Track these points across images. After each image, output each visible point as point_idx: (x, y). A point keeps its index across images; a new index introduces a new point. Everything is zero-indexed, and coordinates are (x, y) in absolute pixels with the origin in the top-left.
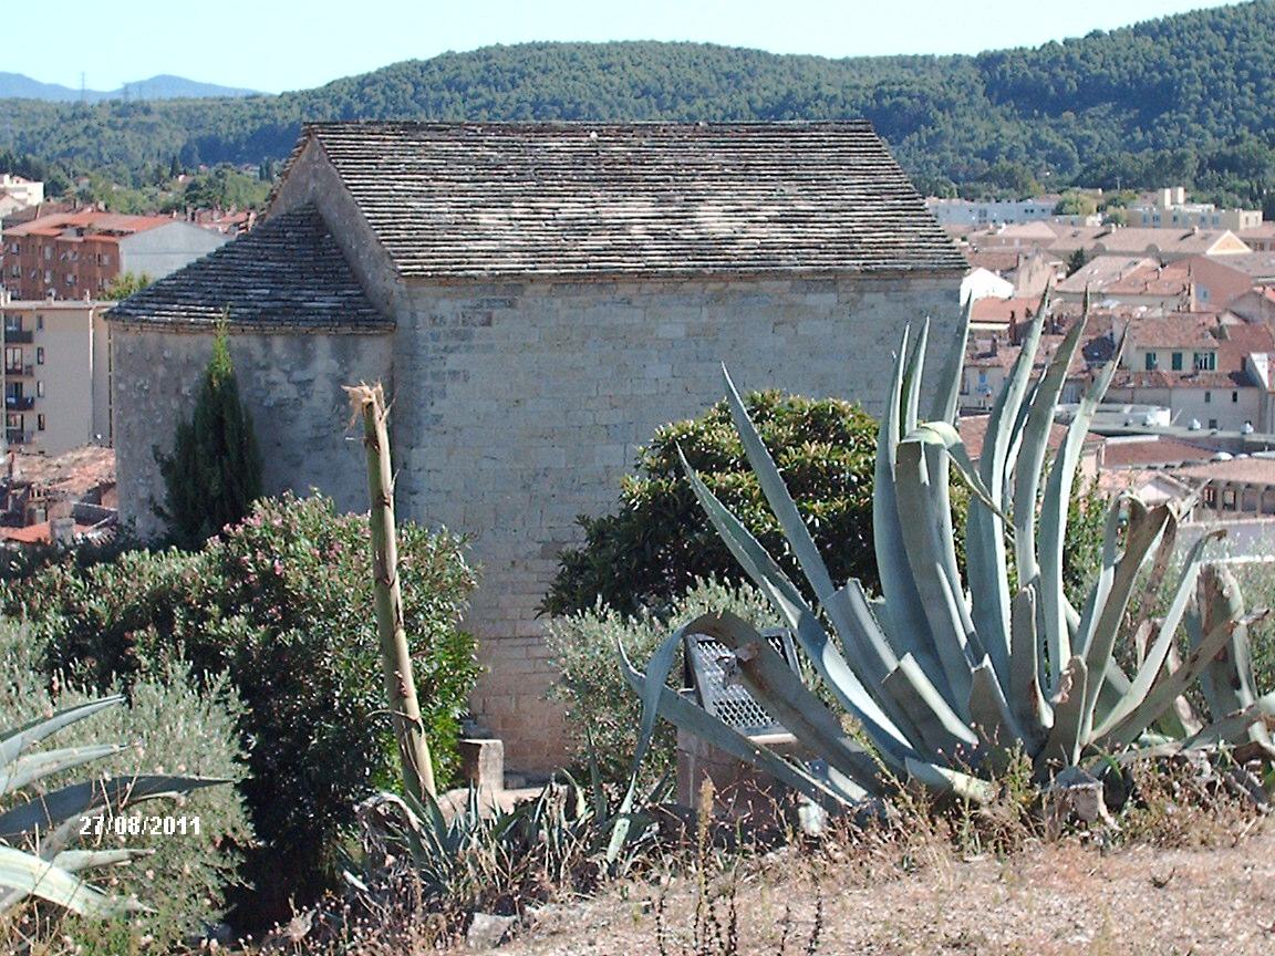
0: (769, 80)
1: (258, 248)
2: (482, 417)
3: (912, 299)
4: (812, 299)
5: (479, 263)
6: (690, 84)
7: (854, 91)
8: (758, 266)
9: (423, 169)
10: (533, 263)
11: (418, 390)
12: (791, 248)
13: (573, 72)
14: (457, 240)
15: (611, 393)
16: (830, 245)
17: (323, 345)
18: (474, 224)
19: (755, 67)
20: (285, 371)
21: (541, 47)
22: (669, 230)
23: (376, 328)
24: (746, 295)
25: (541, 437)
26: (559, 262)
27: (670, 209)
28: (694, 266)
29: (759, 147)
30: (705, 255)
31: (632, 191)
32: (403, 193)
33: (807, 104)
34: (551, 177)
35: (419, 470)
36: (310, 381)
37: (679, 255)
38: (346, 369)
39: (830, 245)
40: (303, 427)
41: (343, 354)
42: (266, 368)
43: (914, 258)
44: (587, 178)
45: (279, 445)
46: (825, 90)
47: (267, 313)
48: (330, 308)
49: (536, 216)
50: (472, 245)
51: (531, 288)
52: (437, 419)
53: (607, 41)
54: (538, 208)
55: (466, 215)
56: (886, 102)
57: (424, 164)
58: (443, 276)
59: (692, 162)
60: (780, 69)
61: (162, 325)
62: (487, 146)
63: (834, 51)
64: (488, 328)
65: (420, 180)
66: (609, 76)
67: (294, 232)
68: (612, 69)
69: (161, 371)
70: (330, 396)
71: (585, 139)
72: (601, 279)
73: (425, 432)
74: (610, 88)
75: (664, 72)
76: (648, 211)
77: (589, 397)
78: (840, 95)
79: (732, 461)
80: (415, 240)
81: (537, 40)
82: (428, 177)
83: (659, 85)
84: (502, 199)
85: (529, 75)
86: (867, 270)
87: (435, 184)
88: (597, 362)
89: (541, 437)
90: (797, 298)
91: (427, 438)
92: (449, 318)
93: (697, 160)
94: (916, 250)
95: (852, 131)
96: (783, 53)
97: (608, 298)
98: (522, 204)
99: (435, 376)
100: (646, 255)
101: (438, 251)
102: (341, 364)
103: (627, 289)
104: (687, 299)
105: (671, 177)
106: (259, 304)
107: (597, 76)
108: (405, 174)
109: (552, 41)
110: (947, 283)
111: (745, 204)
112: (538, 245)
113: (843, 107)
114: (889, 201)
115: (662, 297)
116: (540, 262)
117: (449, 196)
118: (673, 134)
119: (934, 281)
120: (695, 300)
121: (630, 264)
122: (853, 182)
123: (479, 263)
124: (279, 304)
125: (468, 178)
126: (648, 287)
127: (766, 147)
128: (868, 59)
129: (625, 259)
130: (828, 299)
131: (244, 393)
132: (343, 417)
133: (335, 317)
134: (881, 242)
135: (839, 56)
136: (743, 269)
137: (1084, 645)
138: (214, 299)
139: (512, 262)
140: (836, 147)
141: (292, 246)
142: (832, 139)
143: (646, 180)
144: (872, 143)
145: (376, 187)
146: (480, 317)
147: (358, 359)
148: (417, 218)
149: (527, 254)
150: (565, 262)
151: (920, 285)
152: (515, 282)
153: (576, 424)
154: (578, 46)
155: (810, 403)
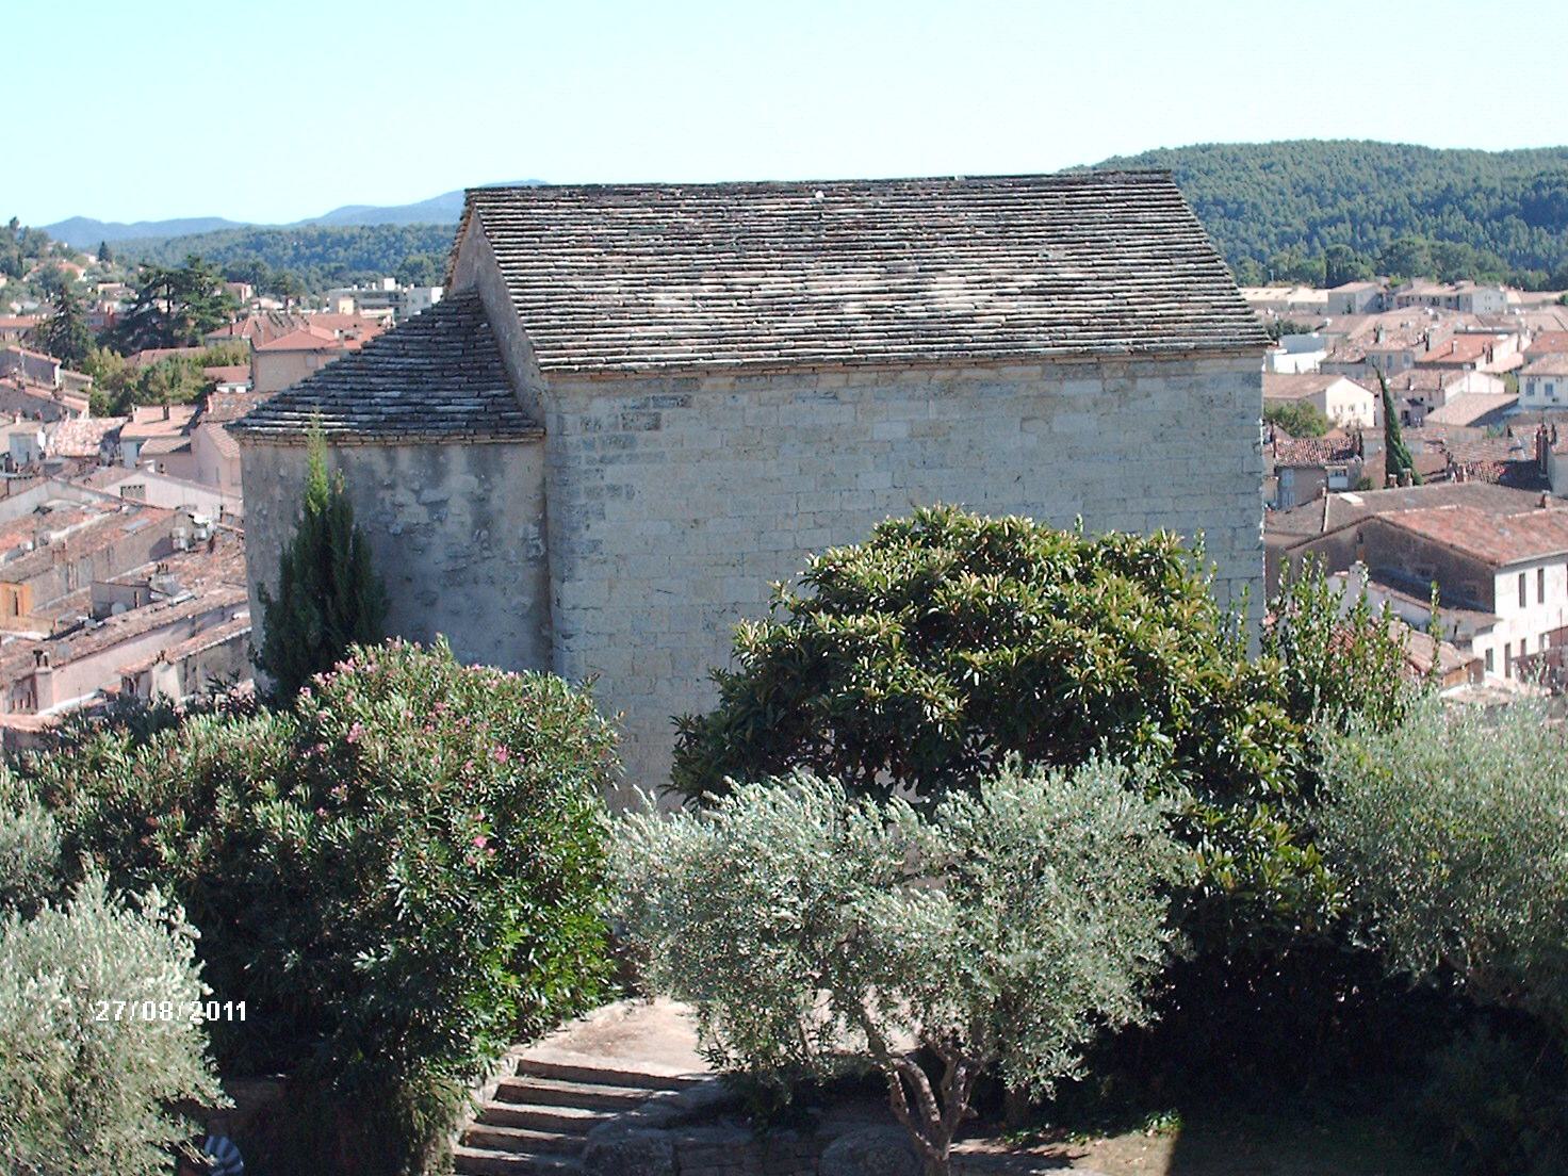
0: (1430, 175)
1: (401, 341)
2: (650, 541)
3: (1200, 385)
4: (1070, 388)
5: (642, 353)
6: (1349, 180)
7: (1513, 183)
8: (998, 348)
9: (598, 241)
10: (710, 351)
11: (569, 511)
12: (1044, 325)
13: (1236, 173)
14: (621, 325)
15: (815, 510)
16: (1095, 321)
17: (457, 457)
18: (647, 305)
19: (1415, 162)
20: (413, 491)
21: (1206, 149)
22: (892, 307)
23: (522, 435)
24: (985, 384)
25: (727, 564)
26: (743, 350)
27: (898, 281)
28: (916, 350)
29: (1025, 204)
30: (933, 336)
31: (856, 260)
32: (566, 271)
33: (1466, 196)
34: (756, 246)
35: (574, 608)
36: (443, 502)
37: (901, 337)
38: (487, 486)
39: (1095, 321)
40: (436, 559)
41: (483, 468)
42: (391, 487)
43: (1200, 334)
44: (801, 246)
45: (409, 580)
46: (1483, 182)
47: (392, 420)
48: (467, 412)
49: (727, 294)
50: (638, 332)
51: (708, 382)
52: (595, 545)
53: (1268, 142)
54: (733, 284)
55: (639, 295)
56: (1545, 193)
57: (602, 235)
58: (594, 370)
59: (937, 224)
60: (1439, 163)
61: (274, 437)
62: (685, 212)
63: (1493, 144)
64: (655, 433)
65: (592, 254)
66: (1271, 176)
67: (445, 321)
68: (1274, 168)
69: (278, 492)
70: (468, 519)
71: (807, 200)
72: (797, 369)
73: (580, 561)
74: (1271, 187)
75: (1325, 169)
76: (870, 284)
77: (787, 515)
78: (1499, 188)
79: (872, 599)
80: (567, 327)
81: (1200, 143)
82: (601, 250)
83: (1319, 183)
84: (688, 274)
85: (1193, 177)
86: (1137, 350)
87: (610, 258)
88: (797, 471)
89: (727, 564)
90: (1051, 387)
91: (582, 570)
92: (605, 422)
93: (943, 222)
94: (1204, 324)
95: (1147, 182)
96: (1443, 147)
97: (809, 392)
98: (715, 280)
99: (590, 492)
100: (856, 339)
101: (593, 340)
102: (481, 480)
103: (832, 381)
104: (910, 392)
105: (907, 243)
106: (384, 409)
107: (1261, 177)
108: (574, 247)
109: (1215, 143)
110: (1245, 364)
111: (995, 273)
112: (722, 330)
113: (1502, 199)
114: (1179, 264)
115: (876, 389)
116: (719, 350)
117: (624, 273)
118: (920, 191)
119: (1227, 362)
120: (920, 392)
121: (834, 349)
122: (1137, 242)
123: (642, 353)
124: (408, 408)
125: (651, 250)
126: (857, 377)
127: (1035, 204)
128: (1527, 152)
129: (829, 343)
130: (1093, 386)
131: (360, 519)
132: (486, 545)
133: (473, 422)
134: (1161, 316)
135: (1498, 148)
136: (977, 352)
137: (519, 1103)
138: (336, 405)
139: (686, 351)
140: (1123, 201)
141: (441, 339)
142: (1119, 191)
143: (876, 247)
144: (1170, 196)
145: (536, 264)
146: (645, 420)
147: (502, 472)
148: (577, 299)
149: (706, 341)
150: (751, 349)
151: (1208, 367)
152: (687, 375)
153: (770, 547)
154: (1241, 147)
155: (977, 523)
